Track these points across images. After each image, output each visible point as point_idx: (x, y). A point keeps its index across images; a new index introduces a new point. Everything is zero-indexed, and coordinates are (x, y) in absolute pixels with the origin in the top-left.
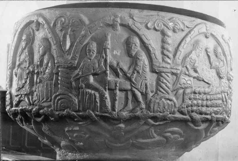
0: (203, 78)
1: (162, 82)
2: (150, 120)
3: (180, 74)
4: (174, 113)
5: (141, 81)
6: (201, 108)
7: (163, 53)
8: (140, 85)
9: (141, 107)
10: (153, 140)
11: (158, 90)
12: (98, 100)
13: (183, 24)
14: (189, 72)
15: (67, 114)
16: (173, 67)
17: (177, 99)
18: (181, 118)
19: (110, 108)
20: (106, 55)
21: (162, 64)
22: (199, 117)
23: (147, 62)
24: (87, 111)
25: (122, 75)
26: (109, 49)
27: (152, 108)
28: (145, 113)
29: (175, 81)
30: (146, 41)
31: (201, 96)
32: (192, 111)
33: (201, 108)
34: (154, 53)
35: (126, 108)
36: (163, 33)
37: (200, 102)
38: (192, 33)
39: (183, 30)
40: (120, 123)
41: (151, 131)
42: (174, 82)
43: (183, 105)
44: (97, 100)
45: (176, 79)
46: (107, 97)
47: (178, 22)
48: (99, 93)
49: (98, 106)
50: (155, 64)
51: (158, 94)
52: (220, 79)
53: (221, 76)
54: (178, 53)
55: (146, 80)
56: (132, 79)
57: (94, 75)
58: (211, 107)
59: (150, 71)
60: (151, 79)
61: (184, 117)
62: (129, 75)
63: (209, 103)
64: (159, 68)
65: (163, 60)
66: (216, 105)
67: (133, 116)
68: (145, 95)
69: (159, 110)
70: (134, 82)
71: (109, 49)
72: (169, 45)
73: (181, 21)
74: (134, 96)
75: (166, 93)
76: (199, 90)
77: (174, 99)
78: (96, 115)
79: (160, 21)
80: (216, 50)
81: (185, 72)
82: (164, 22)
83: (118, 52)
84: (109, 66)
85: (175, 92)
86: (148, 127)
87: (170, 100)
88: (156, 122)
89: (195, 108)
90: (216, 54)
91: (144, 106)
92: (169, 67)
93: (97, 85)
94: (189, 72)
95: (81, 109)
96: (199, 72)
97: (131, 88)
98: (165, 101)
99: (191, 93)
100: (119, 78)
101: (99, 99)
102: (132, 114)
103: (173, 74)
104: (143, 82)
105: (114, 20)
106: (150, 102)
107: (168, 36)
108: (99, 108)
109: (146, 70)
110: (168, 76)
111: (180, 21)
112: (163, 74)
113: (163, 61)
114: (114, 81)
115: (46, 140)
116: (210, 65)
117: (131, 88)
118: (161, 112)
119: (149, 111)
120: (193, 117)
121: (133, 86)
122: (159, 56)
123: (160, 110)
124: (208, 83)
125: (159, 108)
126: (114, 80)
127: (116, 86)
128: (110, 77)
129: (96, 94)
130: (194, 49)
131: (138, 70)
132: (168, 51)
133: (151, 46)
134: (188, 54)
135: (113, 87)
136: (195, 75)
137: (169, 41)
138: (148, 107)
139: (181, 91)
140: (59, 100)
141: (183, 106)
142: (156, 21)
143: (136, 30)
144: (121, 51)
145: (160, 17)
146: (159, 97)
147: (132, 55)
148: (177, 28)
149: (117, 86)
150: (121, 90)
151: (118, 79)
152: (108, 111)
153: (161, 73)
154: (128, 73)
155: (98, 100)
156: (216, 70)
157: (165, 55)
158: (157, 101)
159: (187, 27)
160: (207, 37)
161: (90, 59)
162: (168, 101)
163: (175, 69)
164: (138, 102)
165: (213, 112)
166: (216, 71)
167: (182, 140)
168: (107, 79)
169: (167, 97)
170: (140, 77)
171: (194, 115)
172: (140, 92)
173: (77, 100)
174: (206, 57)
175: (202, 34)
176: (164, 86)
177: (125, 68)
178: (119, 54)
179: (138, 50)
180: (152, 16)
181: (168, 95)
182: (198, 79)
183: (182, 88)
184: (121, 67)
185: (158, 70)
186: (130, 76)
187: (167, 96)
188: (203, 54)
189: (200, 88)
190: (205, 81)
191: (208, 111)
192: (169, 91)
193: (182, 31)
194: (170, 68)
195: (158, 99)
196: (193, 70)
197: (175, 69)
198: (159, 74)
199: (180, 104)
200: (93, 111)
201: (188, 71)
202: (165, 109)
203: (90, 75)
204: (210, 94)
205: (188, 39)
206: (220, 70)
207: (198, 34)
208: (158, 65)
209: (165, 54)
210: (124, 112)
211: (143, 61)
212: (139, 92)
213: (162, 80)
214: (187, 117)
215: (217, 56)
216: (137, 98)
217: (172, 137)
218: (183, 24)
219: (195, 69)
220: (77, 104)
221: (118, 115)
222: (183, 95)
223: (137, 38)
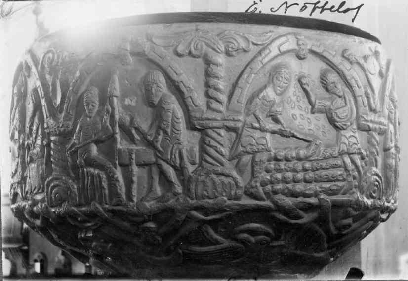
0: (292, 132)
1: (209, 146)
2: (195, 213)
3: (243, 128)
4: (237, 198)
5: (171, 145)
6: (294, 186)
7: (207, 95)
8: (170, 153)
9: (175, 192)
10: (218, 247)
11: (203, 160)
12: (105, 184)
14: (260, 123)
15: (65, 211)
16: (228, 117)
17: (240, 172)
19: (124, 196)
21: (206, 113)
22: (290, 202)
23: (180, 113)
24: (92, 203)
25: (139, 138)
26: (116, 97)
27: (193, 191)
28: (181, 200)
29: (235, 141)
30: (175, 77)
31: (291, 164)
33: (294, 186)
34: (191, 97)
36: (208, 62)
37: (290, 175)
39: (245, 51)
42: (232, 144)
43: (253, 182)
44: (103, 184)
45: (236, 138)
46: (117, 178)
47: (235, 38)
48: (107, 174)
49: (105, 194)
50: (193, 114)
51: (203, 167)
52: (337, 131)
53: (337, 124)
54: (237, 92)
55: (180, 144)
56: (155, 144)
57: (97, 142)
58: (315, 182)
59: (187, 128)
60: (188, 140)
62: (150, 138)
63: (310, 175)
64: (201, 122)
66: (326, 179)
68: (180, 170)
69: (207, 195)
70: (161, 149)
71: (116, 97)
72: (219, 80)
73: (241, 34)
74: (162, 173)
75: (218, 164)
77: (235, 174)
79: (199, 40)
80: (324, 79)
81: (252, 124)
82: (207, 42)
83: (131, 100)
84: (119, 126)
85: (235, 161)
87: (227, 176)
88: (207, 215)
89: (279, 187)
90: (325, 86)
91: (179, 189)
92: (219, 119)
93: (102, 159)
94: (260, 123)
95: (83, 201)
96: (282, 121)
97: (157, 161)
98: (215, 178)
99: (269, 160)
100: (135, 144)
101: (106, 183)
102: (161, 203)
103: (228, 129)
104: (175, 148)
106: (189, 181)
107: (216, 64)
108: (107, 198)
109: (179, 127)
110: (219, 134)
111: (239, 35)
112: (210, 131)
113: (208, 108)
114: (127, 150)
116: (310, 107)
117: (157, 161)
118: (209, 198)
119: (189, 197)
121: (159, 157)
122: (199, 99)
123: (208, 193)
125: (206, 190)
126: (128, 149)
128: (121, 144)
129: (101, 176)
130: (271, 82)
131: (165, 128)
132: (217, 89)
133: (184, 85)
134: (257, 92)
135: (127, 161)
136: (276, 127)
137: (221, 72)
138: (187, 191)
139: (247, 159)
140: (53, 188)
141: (253, 184)
142: (192, 40)
144: (137, 98)
145: (200, 33)
146: (205, 172)
147: (154, 104)
148: (232, 48)
149: (133, 159)
150: (139, 165)
151: (134, 146)
152: (120, 201)
153: (207, 130)
154: (149, 134)
155: (105, 184)
156: (327, 115)
157: (211, 98)
158: (203, 178)
159: (254, 44)
160: (300, 58)
161: (90, 117)
162: (223, 178)
163: (231, 120)
164: (170, 183)
165: (320, 192)
166: (326, 117)
168: (116, 147)
169: (220, 171)
170: (168, 139)
171: (279, 198)
172: (172, 166)
173: (75, 187)
174: (301, 93)
175: (290, 54)
176: (212, 151)
177: (145, 127)
178: (134, 104)
181: (222, 167)
182: (282, 134)
183: (249, 153)
184: (137, 125)
185: (199, 126)
186: (151, 139)
187: (220, 169)
188: (294, 90)
189: (286, 151)
190: (298, 136)
191: (309, 190)
192: (224, 160)
193: (244, 53)
194: (222, 120)
195: (202, 175)
196: (270, 118)
197: (231, 120)
198: (203, 130)
199: (248, 181)
200: (100, 204)
201: (258, 121)
202: (217, 191)
203: (89, 143)
204: (312, 158)
206: (334, 114)
207: (279, 53)
208: (198, 115)
209: (211, 95)
210: (148, 201)
211: (171, 112)
212: (168, 166)
213: (207, 142)
214: (267, 203)
215: (327, 89)
217: (253, 239)
219: (274, 117)
220: (77, 193)
222: (253, 167)
223: (160, 73)
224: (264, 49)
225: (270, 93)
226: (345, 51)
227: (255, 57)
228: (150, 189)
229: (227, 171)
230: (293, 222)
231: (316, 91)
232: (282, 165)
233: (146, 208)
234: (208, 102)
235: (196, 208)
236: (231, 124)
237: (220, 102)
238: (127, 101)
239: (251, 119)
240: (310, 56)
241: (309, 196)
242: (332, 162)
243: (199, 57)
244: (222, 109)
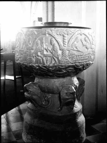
4: (69, 64)
13: (71, 31)
20: (43, 45)
31: (79, 57)
32: (76, 62)
36: (63, 36)
38: (74, 34)
39: (71, 34)
40: (50, 68)
61: (73, 65)
63: (82, 59)
65: (64, 46)
78: (41, 66)
103: (68, 50)
105: (45, 33)
110: (66, 51)
122: (62, 44)
124: (82, 52)
127: (47, 56)
132: (65, 42)
136: (76, 50)
137: (66, 38)
143: (53, 35)
159: (73, 32)
177: (50, 49)
179: (54, 43)
180: (59, 30)
182: (78, 51)
188: (80, 42)
205: (73, 37)
214: (74, 64)
218: (71, 31)
224: (74, 34)
225: (75, 43)
226: (89, 33)
227: (73, 35)
228: (51, 62)
229: (67, 59)
230: (78, 68)
231: (84, 43)
232: (77, 57)
233: (50, 66)
234: (63, 45)
235: (61, 66)
236: (68, 49)
237: (66, 45)
238: (46, 44)
239: (72, 48)
240: (83, 35)
241: (82, 63)
242: (86, 56)
243: (62, 35)
244: (66, 46)
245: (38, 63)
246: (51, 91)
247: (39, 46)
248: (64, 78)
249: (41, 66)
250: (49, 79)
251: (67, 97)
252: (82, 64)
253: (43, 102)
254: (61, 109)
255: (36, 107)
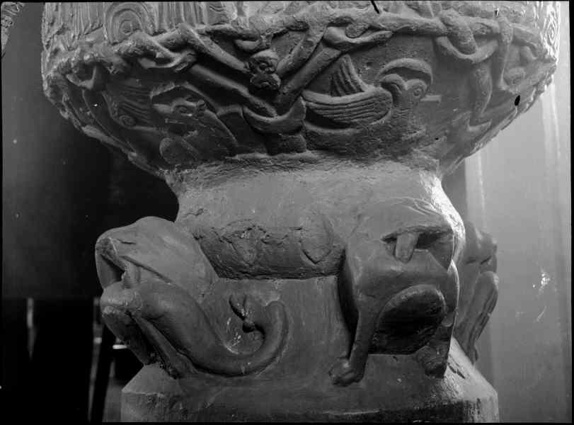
10: (358, 96)
18: (416, 22)
35: (332, 279)
41: (347, 67)
61: (424, 20)
67: (289, 21)
76: (411, 158)
86: (335, 53)
115: (133, 151)
120: (449, 19)
167: (438, 102)
216: (339, 295)
221: (251, 23)
245: (179, 20)
246: (281, 263)
247: (154, 393)
248: (368, 164)
249: (197, 36)
250: (263, 176)
251: (397, 268)
252: (486, 21)
253: (230, 337)
254: (360, 368)
255: (177, 375)
